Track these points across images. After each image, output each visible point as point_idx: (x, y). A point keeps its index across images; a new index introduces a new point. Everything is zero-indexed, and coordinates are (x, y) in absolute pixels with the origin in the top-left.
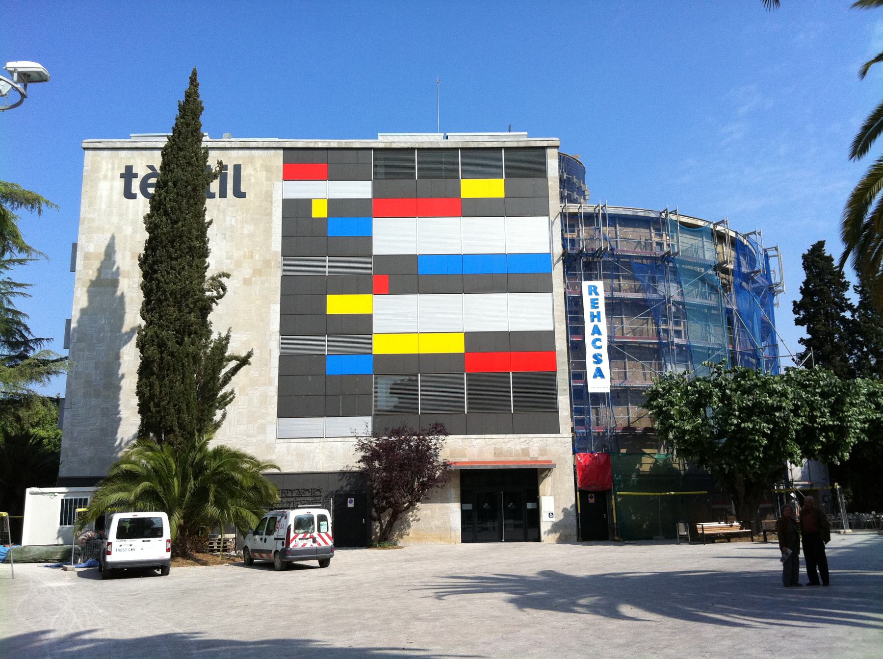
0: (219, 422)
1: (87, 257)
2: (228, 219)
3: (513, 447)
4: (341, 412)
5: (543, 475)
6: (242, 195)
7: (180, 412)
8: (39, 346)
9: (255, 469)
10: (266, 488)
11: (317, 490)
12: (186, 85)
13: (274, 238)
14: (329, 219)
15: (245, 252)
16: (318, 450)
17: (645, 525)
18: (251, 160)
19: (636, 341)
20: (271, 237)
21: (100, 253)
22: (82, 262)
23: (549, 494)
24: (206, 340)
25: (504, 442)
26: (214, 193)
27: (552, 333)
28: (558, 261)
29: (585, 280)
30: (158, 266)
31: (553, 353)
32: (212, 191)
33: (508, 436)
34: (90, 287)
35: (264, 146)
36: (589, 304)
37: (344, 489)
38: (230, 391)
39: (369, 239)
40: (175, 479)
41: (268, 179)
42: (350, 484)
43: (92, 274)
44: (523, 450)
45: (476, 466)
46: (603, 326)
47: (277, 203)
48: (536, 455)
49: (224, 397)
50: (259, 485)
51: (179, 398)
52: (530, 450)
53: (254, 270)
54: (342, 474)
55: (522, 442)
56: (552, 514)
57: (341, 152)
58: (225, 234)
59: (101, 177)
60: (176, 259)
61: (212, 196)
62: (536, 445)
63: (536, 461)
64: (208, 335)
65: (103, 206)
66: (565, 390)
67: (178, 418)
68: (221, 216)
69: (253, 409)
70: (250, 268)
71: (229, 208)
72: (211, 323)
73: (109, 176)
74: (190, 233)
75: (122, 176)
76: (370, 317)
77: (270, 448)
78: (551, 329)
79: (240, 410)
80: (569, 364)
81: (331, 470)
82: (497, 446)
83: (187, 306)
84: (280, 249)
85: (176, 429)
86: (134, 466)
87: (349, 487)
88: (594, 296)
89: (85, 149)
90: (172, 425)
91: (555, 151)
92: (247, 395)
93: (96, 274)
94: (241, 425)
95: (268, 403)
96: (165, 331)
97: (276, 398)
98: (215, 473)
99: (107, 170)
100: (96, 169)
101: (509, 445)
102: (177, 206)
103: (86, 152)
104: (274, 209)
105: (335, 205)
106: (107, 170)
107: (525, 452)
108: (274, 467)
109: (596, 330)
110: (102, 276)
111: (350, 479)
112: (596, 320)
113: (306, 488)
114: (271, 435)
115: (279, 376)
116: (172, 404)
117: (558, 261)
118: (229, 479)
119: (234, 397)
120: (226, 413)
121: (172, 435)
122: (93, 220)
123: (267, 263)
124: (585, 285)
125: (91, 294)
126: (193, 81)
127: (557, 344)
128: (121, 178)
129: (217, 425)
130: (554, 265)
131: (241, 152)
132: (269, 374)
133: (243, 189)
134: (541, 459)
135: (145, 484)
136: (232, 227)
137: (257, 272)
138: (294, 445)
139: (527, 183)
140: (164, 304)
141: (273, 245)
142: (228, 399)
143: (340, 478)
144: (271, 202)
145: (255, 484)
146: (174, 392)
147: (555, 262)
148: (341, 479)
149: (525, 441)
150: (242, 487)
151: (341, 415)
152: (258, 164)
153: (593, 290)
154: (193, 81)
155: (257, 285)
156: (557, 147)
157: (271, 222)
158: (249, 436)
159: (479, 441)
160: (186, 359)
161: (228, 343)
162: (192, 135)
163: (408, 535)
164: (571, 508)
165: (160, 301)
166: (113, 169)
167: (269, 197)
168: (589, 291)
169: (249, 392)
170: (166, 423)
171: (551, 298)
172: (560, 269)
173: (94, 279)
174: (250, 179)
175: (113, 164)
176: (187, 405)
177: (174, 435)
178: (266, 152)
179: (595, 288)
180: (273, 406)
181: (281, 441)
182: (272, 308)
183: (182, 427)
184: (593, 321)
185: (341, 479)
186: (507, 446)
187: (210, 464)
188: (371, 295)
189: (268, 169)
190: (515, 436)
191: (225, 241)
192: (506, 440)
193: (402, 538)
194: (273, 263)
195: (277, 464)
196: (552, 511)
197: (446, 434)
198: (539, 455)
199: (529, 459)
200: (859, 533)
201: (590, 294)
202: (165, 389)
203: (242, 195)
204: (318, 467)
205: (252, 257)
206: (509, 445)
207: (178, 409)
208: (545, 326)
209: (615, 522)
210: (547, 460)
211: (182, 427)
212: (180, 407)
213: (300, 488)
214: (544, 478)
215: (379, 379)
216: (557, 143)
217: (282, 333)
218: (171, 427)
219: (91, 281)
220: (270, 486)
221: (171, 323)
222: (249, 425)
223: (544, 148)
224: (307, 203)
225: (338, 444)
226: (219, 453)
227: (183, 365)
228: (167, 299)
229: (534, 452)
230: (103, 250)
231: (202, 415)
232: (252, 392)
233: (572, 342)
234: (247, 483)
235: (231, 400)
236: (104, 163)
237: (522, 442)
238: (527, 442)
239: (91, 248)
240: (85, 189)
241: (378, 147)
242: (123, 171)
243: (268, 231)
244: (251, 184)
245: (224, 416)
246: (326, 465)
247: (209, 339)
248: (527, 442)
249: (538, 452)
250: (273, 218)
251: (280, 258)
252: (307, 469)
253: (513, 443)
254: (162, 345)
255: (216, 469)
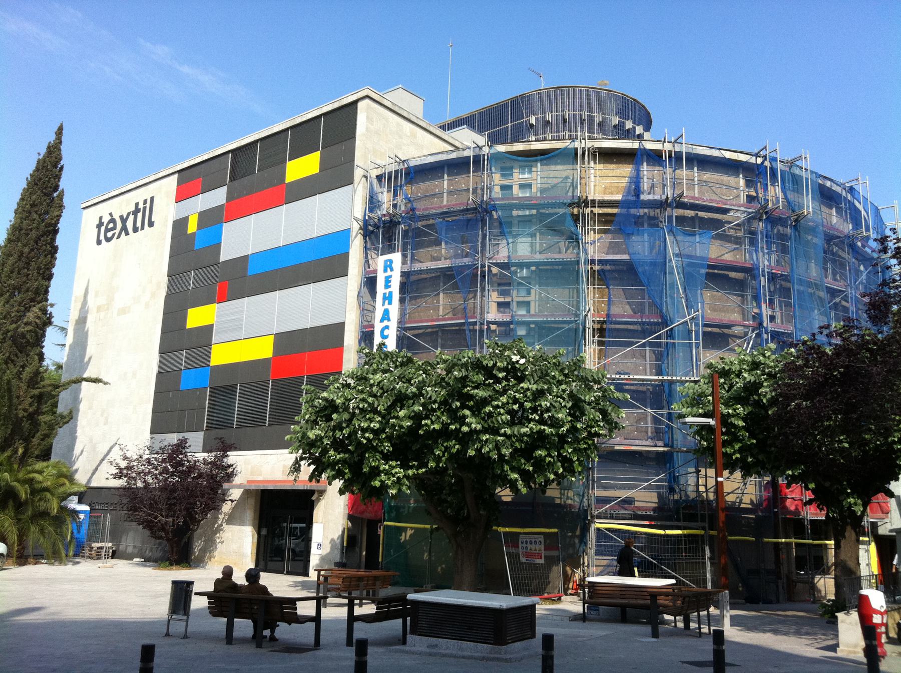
12: (52, 138)
17: (439, 568)
19: (420, 324)
23: (320, 521)
46: (394, 309)
56: (321, 545)
88: (389, 273)
109: (386, 316)
112: (387, 302)
126: (60, 132)
153: (388, 266)
154: (60, 132)
163: (214, 557)
164: (338, 538)
193: (210, 560)
196: (320, 541)
200: (118, 617)
209: (380, 560)
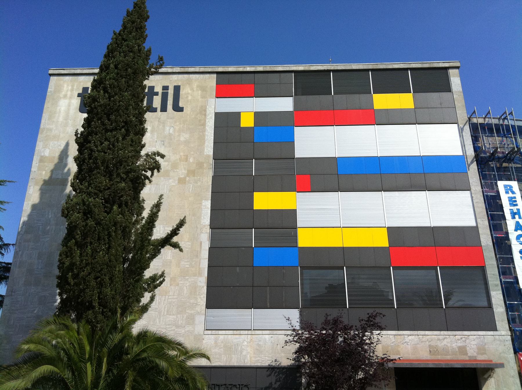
0: (147, 305)
1: (42, 160)
2: (168, 128)
3: (449, 345)
4: (268, 304)
5: (486, 376)
6: (181, 110)
7: (102, 286)
8: (6, 250)
9: (182, 358)
10: (194, 380)
11: (245, 386)
13: (206, 144)
14: (255, 127)
15: (181, 156)
16: (246, 343)
18: (189, 82)
20: (204, 143)
21: (54, 157)
22: (37, 164)
24: (138, 216)
25: (439, 339)
26: (156, 108)
27: (475, 229)
28: (472, 162)
29: (499, 180)
30: (104, 174)
31: (479, 246)
32: (154, 106)
33: (442, 333)
34: (43, 185)
35: (200, 71)
36: (508, 203)
37: (273, 386)
38: (160, 273)
39: (291, 143)
40: (89, 365)
41: (203, 97)
42: (279, 381)
43: (45, 175)
44: (460, 348)
45: (416, 365)
47: (210, 116)
48: (475, 354)
49: (154, 278)
50: (186, 376)
51: (102, 269)
52: (468, 348)
53: (188, 171)
54: (271, 369)
55: (458, 340)
57: (266, 75)
58: (163, 141)
59: (61, 96)
60: (111, 131)
61: (155, 110)
62: (473, 343)
63: (448, 364)
64: (139, 210)
65: (61, 119)
66: (497, 285)
67: (100, 293)
68: (161, 127)
69: (183, 299)
70: (185, 169)
71: (169, 120)
72: (144, 200)
73: (68, 96)
74: (127, 109)
75: (79, 95)
76: (295, 211)
77: (199, 338)
78: (473, 224)
79: (170, 300)
80: (497, 260)
81: (259, 364)
82: (431, 343)
83: (118, 175)
84: (211, 153)
85: (96, 304)
86: (40, 347)
87: (278, 383)
89: (51, 75)
90: (92, 300)
91: (456, 71)
92: (178, 285)
93: (49, 175)
94: (170, 315)
95: (198, 294)
96: (92, 198)
97: (205, 288)
98: (137, 359)
99: (67, 91)
100: (58, 89)
101: (445, 342)
102: (116, 83)
103: (52, 78)
104: (207, 121)
105: (259, 116)
106: (67, 91)
107: (463, 350)
108: (203, 356)
110: (54, 176)
111: (279, 374)
112: (517, 216)
113: (234, 384)
114: (200, 328)
115: (209, 266)
116: (93, 275)
117: (472, 162)
118: (152, 368)
119: (164, 280)
120: (155, 295)
121: (90, 312)
122: (51, 130)
123: (200, 165)
124: (501, 185)
125: (43, 192)
127: (482, 240)
128: (78, 96)
129: (145, 309)
130: (469, 166)
131: (180, 76)
132: (199, 265)
133: (181, 105)
134: (481, 358)
135: (45, 369)
136: (170, 135)
137: (191, 173)
138: (222, 337)
139: (434, 98)
140: (95, 172)
141: (205, 150)
142: (158, 282)
143: (268, 373)
144: (205, 115)
145: (182, 376)
146: (97, 262)
147: (469, 163)
148: (270, 375)
149: (461, 338)
150: (167, 378)
151: (269, 306)
152: (195, 85)
155: (191, 183)
156: (458, 68)
157: (205, 131)
158: (178, 326)
159: (413, 337)
160: (113, 228)
161: (159, 211)
162: (137, 31)
165: (91, 170)
166: (72, 90)
167: (203, 111)
168: (506, 190)
169: (180, 282)
170: (85, 297)
171: (469, 195)
172: (475, 169)
173: (47, 178)
174: (187, 97)
175: (73, 86)
176: (110, 279)
177: (93, 312)
178: (202, 76)
179: (511, 187)
180: (202, 296)
181: (209, 332)
182: (203, 204)
183: (103, 304)
184: (514, 218)
185: (270, 375)
186: (443, 344)
187: (132, 348)
188: (294, 193)
189: (203, 89)
190: (449, 333)
191: (163, 147)
192: (441, 337)
194: (205, 165)
195: (208, 353)
197: (381, 329)
198: (478, 354)
199: (467, 359)
201: (507, 193)
202: (87, 258)
203: (181, 110)
204: (246, 361)
205: (186, 160)
206: (445, 342)
207: (100, 282)
208: (469, 221)
210: (487, 359)
211: (103, 304)
212: (103, 280)
213: (228, 383)
214: (486, 380)
215: (305, 271)
216: (458, 64)
217: (213, 227)
218: (91, 303)
219: (45, 181)
220: (198, 378)
221: (101, 192)
222: (179, 316)
223: (446, 69)
224: (237, 115)
225: (267, 337)
226: (143, 335)
227: (109, 235)
228: (97, 168)
229: (472, 351)
230: (57, 154)
231: (127, 291)
232: (181, 282)
233: (496, 237)
234: (173, 373)
235: (161, 283)
236: (65, 86)
237: (458, 340)
238: (464, 339)
239: (47, 153)
240: (48, 105)
241: (298, 69)
242: (81, 92)
243: (202, 139)
244: (188, 101)
245: (152, 299)
246: (253, 359)
247: (141, 215)
248: (464, 339)
249: (476, 350)
250: (207, 128)
251: (211, 161)
252: (235, 362)
253: (449, 340)
254: (87, 213)
255: (138, 355)
